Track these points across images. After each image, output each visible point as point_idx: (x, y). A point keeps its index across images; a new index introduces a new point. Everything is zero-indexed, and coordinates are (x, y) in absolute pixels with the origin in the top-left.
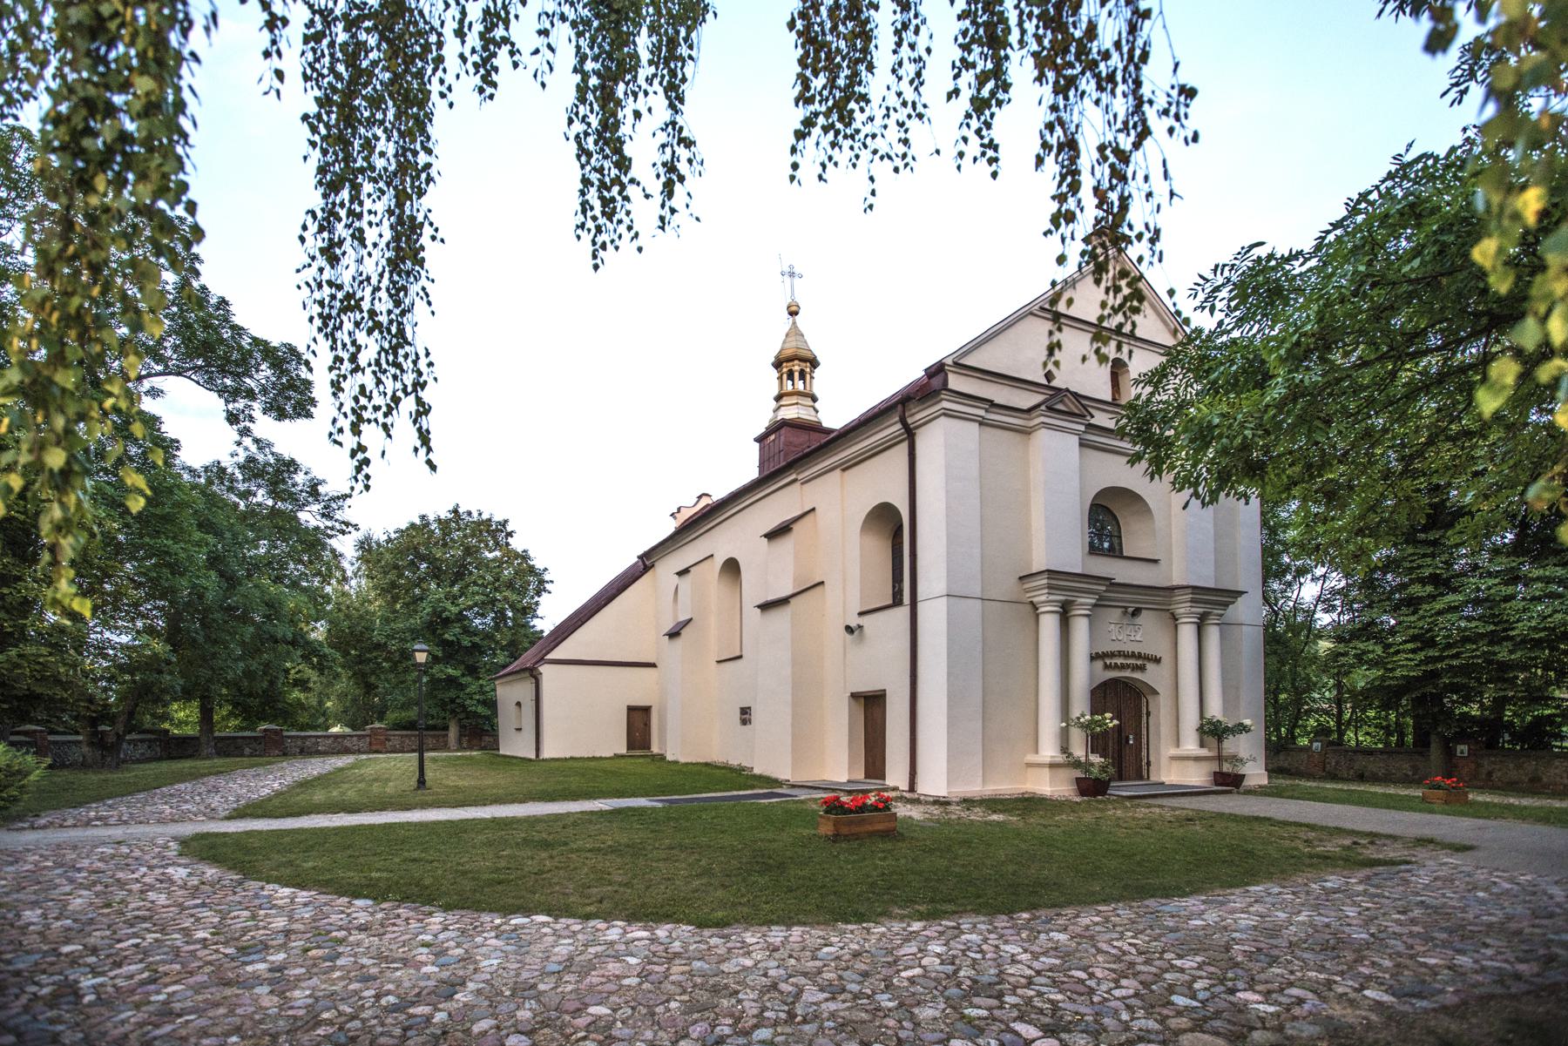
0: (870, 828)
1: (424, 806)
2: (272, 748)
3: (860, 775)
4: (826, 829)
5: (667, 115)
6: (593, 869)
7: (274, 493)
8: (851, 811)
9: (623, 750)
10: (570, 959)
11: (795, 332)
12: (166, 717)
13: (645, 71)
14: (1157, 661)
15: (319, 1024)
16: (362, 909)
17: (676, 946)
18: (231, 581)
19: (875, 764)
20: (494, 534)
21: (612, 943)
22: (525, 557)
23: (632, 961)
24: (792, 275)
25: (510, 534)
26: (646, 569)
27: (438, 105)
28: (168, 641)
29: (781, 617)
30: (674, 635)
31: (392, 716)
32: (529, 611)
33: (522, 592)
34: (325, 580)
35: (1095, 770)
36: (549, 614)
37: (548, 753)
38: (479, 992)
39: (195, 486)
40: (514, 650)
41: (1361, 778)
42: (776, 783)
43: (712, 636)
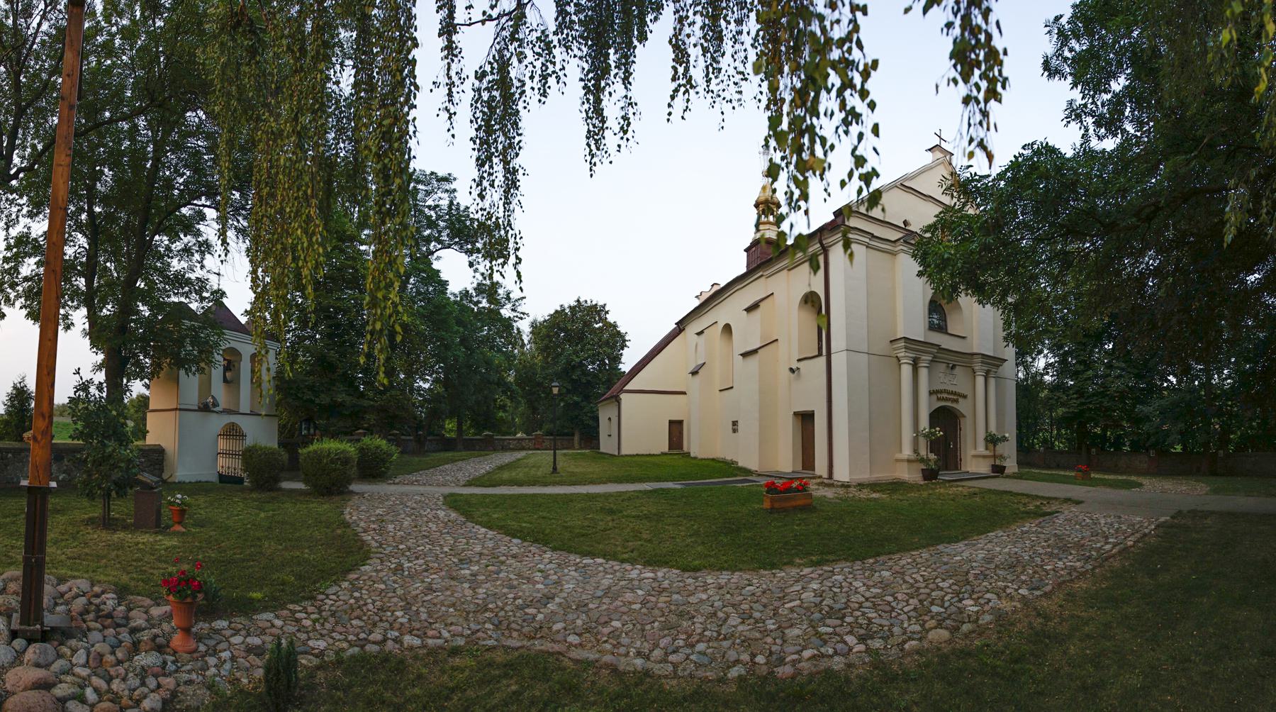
0: (793, 503)
1: (555, 484)
2: (488, 446)
4: (767, 505)
5: (624, 92)
6: (633, 530)
8: (781, 492)
9: (666, 449)
10: (609, 588)
12: (443, 427)
13: (614, 71)
15: (486, 610)
16: (515, 545)
17: (666, 584)
20: (599, 313)
21: (632, 580)
22: (614, 326)
23: (640, 592)
27: (523, 113)
29: (753, 361)
30: (694, 373)
31: (547, 427)
32: (617, 359)
33: (613, 347)
34: (514, 348)
35: (932, 463)
36: (628, 361)
37: (624, 452)
38: (560, 604)
39: (455, 302)
40: (609, 384)
41: (1058, 467)
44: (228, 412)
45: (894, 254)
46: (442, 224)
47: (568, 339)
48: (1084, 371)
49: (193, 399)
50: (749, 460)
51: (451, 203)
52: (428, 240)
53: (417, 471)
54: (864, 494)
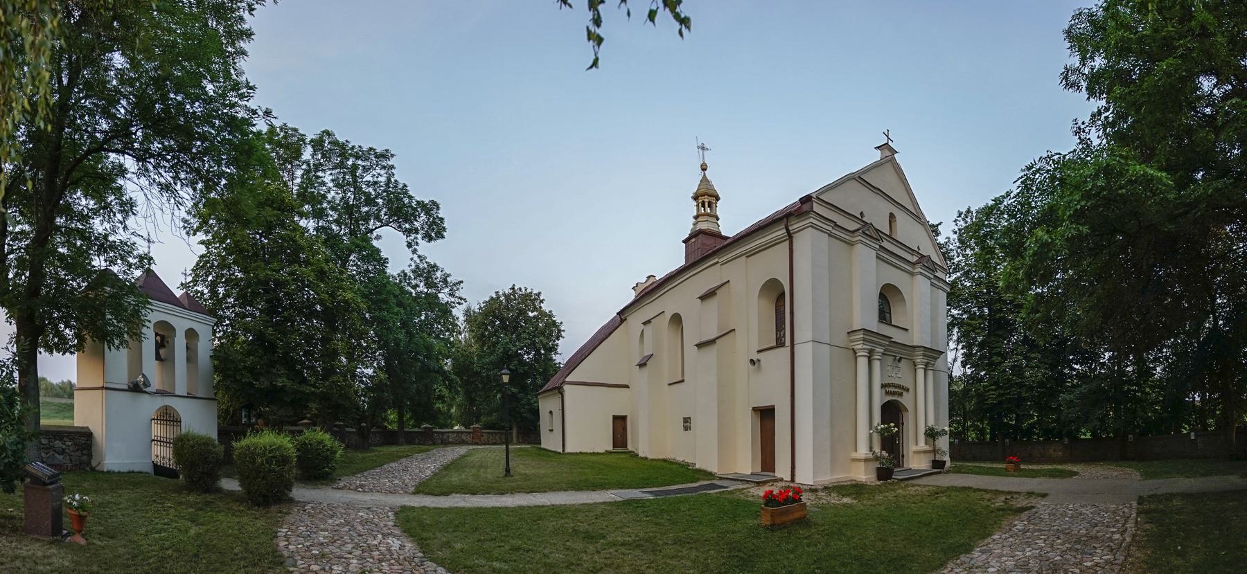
0: (791, 517)
1: (513, 491)
2: (428, 440)
3: (759, 470)
4: (766, 520)
7: (428, 285)
9: (610, 448)
11: (705, 180)
12: (385, 419)
18: (410, 335)
19: (768, 462)
22: (550, 315)
24: (703, 148)
25: (542, 301)
26: (622, 321)
28: (386, 372)
29: (711, 353)
30: (642, 365)
31: (483, 419)
32: (553, 349)
36: (565, 351)
37: (568, 450)
41: (974, 459)
42: (710, 475)
43: (666, 366)
44: (161, 393)
45: (851, 244)
46: (380, 201)
47: (504, 327)
48: (1001, 363)
49: (121, 376)
50: (707, 461)
51: (389, 180)
52: (366, 219)
53: (362, 471)
54: (834, 499)
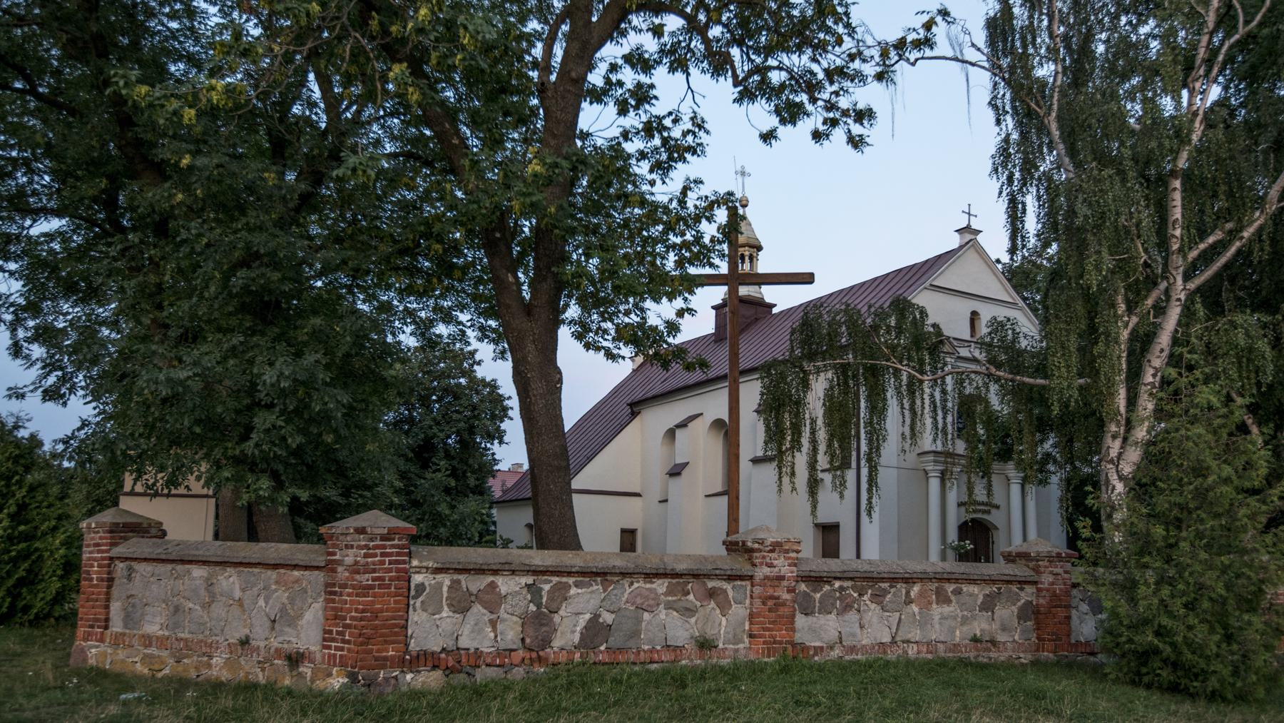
14: (997, 507)
24: (743, 174)
